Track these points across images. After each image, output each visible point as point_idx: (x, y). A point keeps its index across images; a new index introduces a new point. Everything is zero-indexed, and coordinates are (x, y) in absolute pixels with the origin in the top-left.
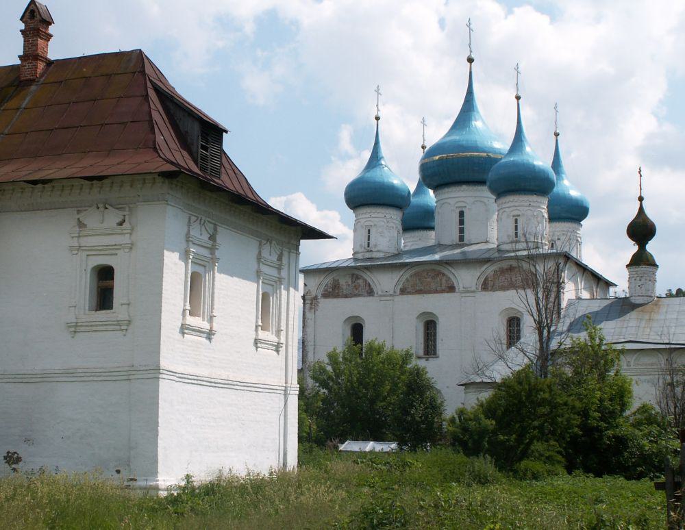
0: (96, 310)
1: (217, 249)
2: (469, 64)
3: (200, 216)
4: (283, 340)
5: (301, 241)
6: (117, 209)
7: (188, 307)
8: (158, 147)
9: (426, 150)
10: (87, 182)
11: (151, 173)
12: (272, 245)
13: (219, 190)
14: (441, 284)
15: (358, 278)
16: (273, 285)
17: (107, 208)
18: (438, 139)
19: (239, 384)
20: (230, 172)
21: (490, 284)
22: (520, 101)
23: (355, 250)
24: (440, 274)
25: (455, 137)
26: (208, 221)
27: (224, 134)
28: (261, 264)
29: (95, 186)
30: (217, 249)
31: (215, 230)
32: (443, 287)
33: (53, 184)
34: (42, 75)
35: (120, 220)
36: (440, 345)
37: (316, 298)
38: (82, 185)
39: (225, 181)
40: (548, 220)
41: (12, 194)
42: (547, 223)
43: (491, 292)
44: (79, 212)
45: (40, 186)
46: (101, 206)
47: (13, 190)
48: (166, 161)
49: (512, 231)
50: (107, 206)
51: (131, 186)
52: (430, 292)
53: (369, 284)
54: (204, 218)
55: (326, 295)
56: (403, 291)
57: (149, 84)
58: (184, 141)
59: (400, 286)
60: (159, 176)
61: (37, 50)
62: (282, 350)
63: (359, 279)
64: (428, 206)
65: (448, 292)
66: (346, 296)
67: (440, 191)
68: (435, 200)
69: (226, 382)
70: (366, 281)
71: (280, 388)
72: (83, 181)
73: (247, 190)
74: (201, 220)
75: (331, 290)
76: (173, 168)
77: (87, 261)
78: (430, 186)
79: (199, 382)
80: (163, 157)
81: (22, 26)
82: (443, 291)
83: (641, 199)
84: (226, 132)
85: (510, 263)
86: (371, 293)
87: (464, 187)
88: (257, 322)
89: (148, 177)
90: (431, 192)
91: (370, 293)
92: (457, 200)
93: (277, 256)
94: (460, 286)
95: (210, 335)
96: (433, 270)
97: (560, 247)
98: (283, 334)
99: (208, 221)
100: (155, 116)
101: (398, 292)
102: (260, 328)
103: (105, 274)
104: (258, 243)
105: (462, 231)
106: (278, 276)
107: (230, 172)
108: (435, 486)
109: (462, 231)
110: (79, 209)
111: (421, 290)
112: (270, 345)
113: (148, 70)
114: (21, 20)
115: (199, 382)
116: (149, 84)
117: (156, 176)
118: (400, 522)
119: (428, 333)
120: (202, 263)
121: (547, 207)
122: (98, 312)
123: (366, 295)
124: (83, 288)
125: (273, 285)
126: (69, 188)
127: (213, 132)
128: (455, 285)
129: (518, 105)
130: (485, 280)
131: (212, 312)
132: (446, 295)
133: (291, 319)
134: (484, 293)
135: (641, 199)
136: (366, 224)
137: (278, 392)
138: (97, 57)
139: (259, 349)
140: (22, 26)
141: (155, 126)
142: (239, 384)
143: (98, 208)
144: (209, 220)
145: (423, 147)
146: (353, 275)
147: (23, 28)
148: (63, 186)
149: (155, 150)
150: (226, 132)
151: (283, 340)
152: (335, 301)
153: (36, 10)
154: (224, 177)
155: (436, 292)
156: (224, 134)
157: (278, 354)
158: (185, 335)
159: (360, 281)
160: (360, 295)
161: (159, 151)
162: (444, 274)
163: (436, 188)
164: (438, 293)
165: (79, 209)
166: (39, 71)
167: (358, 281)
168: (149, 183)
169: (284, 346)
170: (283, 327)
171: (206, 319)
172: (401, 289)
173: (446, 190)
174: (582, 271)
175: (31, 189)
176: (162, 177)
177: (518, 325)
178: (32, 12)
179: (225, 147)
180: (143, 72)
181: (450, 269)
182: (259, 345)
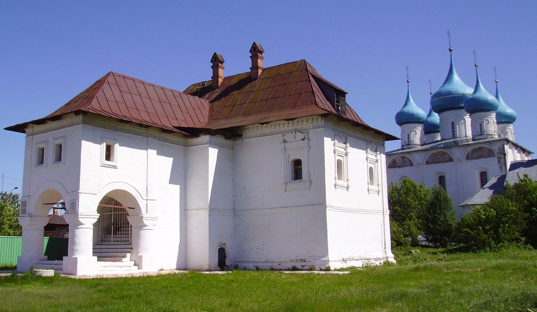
0: (295, 180)
1: (348, 148)
2: (450, 52)
3: (339, 134)
4: (380, 189)
5: (385, 142)
6: (301, 133)
7: (337, 176)
8: (317, 103)
9: (432, 95)
10: (287, 121)
11: (316, 115)
12: (372, 145)
13: (347, 120)
14: (446, 158)
16: (374, 164)
17: (296, 133)
19: (362, 211)
20: (350, 112)
21: (470, 156)
22: (477, 67)
23: (403, 145)
26: (343, 136)
27: (346, 94)
28: (368, 154)
29: (290, 123)
30: (348, 148)
31: (346, 139)
32: (447, 159)
33: (271, 124)
34: (261, 75)
35: (303, 138)
36: (447, 187)
38: (284, 123)
39: (348, 116)
40: (496, 124)
41: (253, 130)
42: (496, 125)
43: (471, 160)
44: (284, 136)
45: (265, 125)
46: (293, 132)
47: (253, 128)
48: (321, 109)
49: (479, 130)
50: (296, 132)
51: (307, 122)
53: (410, 161)
54: (341, 134)
56: (427, 163)
57: (310, 75)
58: (328, 98)
59: (426, 160)
60: (320, 116)
61: (258, 65)
62: (380, 193)
63: (405, 158)
64: (435, 122)
65: (449, 162)
66: (399, 167)
67: (441, 114)
68: (439, 118)
69: (356, 210)
71: (381, 212)
72: (284, 121)
73: (358, 120)
74: (340, 135)
75: (392, 164)
76: (326, 112)
78: (436, 112)
79: (344, 211)
80: (320, 107)
81: (212, 64)
82: (447, 161)
84: (347, 93)
85: (479, 146)
88: (368, 181)
89: (315, 117)
90: (437, 114)
91: (411, 165)
93: (375, 150)
94: (455, 158)
95: (347, 188)
96: (441, 151)
97: (503, 137)
98: (380, 186)
99: (343, 136)
100: (314, 88)
101: (425, 163)
102: (369, 184)
103: (297, 163)
104: (366, 144)
106: (376, 159)
107: (350, 112)
108: (260, 276)
110: (284, 134)
111: (436, 162)
112: (375, 191)
113: (309, 68)
114: (250, 52)
115: (344, 211)
116: (310, 75)
117: (318, 116)
118: (481, 267)
119: (441, 182)
120: (341, 155)
121: (496, 117)
122: (296, 181)
123: (409, 165)
124: (288, 171)
125: (374, 164)
126: (278, 125)
127: (342, 94)
128: (453, 158)
129: (476, 69)
130: (467, 155)
131: (348, 178)
132: (448, 163)
133: (383, 179)
134: (467, 161)
137: (380, 213)
139: (370, 194)
140: (212, 64)
141: (315, 94)
142: (362, 211)
143: (292, 133)
144: (343, 135)
145: (431, 94)
147: (251, 55)
148: (276, 124)
149: (317, 105)
150: (347, 93)
151: (380, 189)
152: (394, 169)
153: (256, 47)
154: (347, 114)
155: (444, 162)
156: (346, 94)
157: (379, 196)
158: (336, 189)
159: (406, 159)
161: (318, 105)
163: (439, 112)
164: (445, 162)
165: (284, 134)
166: (259, 74)
167: (405, 159)
168: (315, 120)
169: (381, 192)
170: (380, 183)
171: (345, 181)
172: (426, 162)
173: (444, 113)
174: (516, 147)
175: (261, 127)
176: (321, 116)
177: (486, 175)
178: (215, 58)
179: (347, 102)
180: (307, 70)
181: (449, 150)
182: (370, 192)
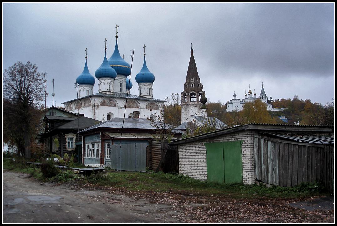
15: (111, 100)
18: (99, 67)
21: (148, 107)
24: (135, 102)
25: (104, 67)
37: (98, 105)
52: (132, 108)
55: (101, 105)
66: (108, 106)
70: (114, 101)
77: (251, 131)
83: (263, 85)
86: (115, 106)
87: (123, 76)
92: (121, 79)
105: (121, 89)
109: (121, 89)
135: (263, 85)
136: (109, 83)
138: (4, 127)
146: (110, 99)
159: (112, 101)
160: (112, 106)
162: (136, 103)
